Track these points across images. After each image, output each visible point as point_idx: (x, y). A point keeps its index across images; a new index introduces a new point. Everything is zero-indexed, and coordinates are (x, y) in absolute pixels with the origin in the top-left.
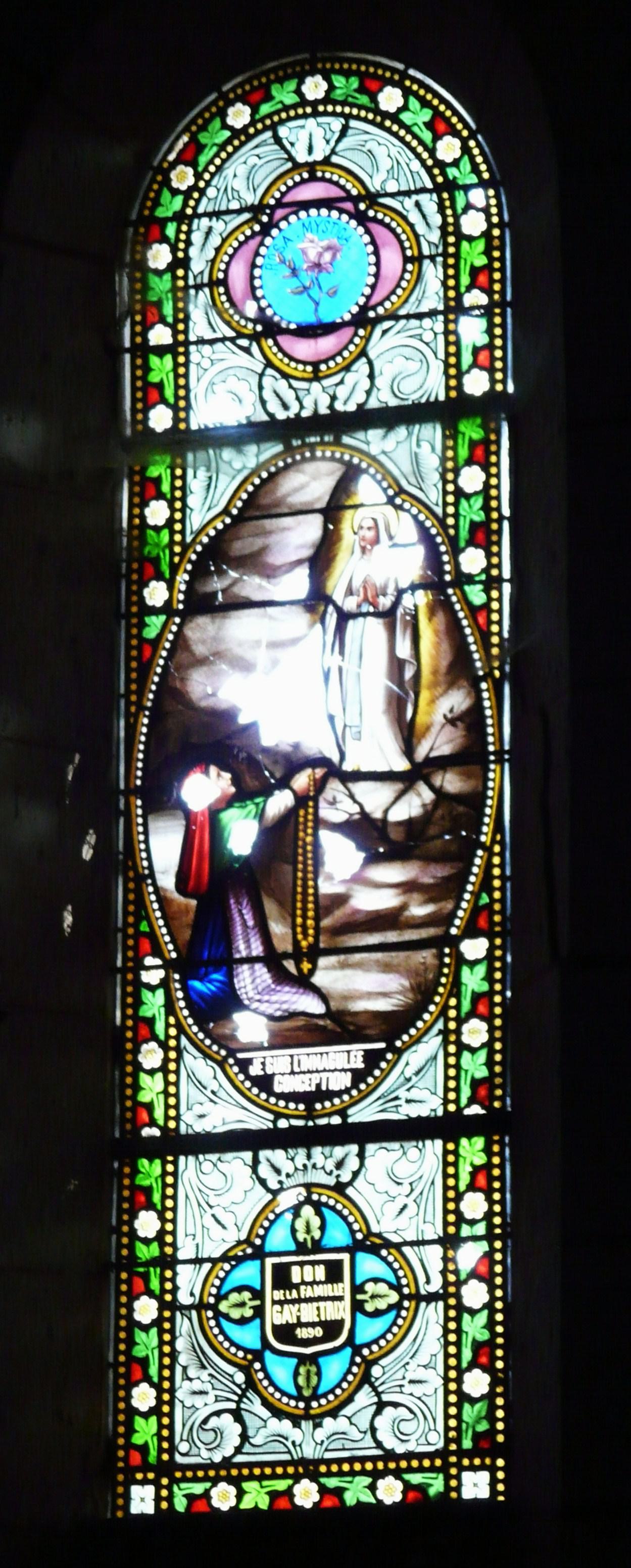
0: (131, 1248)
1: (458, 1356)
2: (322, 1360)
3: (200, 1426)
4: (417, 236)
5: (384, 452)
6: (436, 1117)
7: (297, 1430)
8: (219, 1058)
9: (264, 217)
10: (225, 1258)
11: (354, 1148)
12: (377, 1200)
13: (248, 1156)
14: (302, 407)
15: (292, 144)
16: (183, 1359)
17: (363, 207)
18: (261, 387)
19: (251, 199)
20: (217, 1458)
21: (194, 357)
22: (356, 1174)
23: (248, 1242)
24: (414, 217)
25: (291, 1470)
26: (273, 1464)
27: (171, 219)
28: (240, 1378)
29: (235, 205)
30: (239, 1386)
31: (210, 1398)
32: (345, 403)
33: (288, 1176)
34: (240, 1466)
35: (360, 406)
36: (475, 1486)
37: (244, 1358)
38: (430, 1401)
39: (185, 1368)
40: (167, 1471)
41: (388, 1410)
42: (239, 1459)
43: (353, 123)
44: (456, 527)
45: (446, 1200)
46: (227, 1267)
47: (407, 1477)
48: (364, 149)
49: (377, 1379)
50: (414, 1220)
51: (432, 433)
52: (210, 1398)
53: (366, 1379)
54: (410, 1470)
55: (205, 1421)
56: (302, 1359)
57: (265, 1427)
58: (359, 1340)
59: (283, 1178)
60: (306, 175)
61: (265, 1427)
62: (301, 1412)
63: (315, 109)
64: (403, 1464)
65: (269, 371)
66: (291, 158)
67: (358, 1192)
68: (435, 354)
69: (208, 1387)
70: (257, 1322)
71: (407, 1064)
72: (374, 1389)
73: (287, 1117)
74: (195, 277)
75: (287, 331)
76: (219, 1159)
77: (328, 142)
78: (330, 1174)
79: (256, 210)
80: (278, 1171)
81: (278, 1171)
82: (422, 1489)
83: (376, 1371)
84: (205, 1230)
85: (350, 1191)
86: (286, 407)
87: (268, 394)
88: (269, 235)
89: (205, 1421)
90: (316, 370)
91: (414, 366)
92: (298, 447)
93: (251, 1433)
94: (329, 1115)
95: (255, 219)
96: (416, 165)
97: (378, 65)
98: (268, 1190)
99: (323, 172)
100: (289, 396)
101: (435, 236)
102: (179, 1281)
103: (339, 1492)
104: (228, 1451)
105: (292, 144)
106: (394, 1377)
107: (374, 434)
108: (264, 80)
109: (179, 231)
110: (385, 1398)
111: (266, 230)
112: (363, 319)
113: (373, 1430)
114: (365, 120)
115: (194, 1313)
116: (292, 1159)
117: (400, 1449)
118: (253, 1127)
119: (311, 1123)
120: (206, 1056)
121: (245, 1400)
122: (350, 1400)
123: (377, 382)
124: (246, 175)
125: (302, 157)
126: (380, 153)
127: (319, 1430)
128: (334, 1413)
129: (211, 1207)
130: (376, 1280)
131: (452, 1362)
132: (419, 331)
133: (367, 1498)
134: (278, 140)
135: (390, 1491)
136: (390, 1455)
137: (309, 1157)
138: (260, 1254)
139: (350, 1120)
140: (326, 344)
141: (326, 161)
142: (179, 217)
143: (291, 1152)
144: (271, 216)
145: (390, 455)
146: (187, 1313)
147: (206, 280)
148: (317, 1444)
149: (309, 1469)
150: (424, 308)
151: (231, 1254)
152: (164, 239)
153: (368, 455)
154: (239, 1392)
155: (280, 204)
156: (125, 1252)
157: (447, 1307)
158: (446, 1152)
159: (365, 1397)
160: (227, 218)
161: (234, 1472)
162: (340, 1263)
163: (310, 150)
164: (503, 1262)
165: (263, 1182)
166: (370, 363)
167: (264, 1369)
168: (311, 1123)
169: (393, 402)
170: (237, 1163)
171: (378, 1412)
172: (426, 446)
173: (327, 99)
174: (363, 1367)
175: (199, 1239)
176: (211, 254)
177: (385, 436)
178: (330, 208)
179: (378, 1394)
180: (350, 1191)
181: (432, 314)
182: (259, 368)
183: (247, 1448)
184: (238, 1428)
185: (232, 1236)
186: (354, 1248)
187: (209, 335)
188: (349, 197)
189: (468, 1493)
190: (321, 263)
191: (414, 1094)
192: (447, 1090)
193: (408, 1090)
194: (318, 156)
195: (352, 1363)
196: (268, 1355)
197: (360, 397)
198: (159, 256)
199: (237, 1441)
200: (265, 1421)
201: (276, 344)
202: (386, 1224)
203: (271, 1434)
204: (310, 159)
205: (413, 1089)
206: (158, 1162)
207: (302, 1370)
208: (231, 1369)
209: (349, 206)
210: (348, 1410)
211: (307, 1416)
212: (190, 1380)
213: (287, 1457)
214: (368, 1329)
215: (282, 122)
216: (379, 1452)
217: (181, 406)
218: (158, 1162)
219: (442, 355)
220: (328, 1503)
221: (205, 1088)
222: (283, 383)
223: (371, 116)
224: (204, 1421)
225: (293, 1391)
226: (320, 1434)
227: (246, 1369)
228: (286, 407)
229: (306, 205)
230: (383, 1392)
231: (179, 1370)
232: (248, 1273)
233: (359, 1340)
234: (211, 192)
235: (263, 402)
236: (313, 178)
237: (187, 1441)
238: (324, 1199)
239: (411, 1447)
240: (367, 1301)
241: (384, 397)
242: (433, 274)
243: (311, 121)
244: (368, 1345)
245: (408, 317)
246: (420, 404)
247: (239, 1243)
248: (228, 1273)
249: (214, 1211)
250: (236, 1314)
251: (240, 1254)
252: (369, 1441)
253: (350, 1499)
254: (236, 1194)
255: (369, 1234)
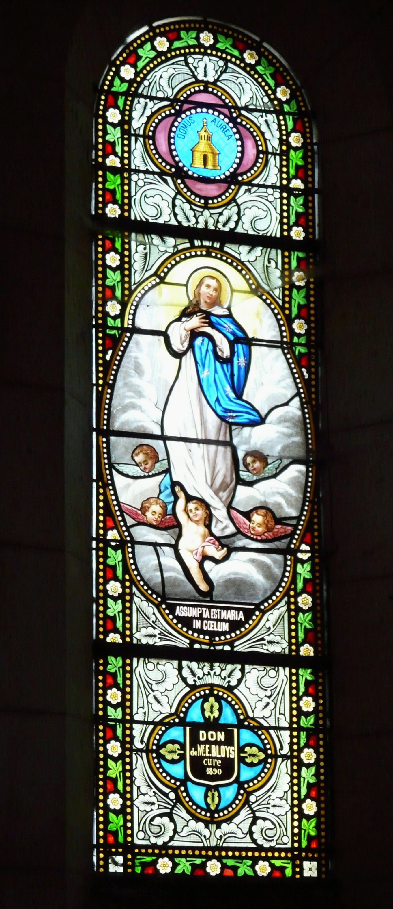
0: (105, 710)
1: (299, 792)
2: (221, 789)
3: (150, 823)
4: (265, 140)
5: (249, 261)
6: (284, 655)
7: (207, 830)
8: (156, 602)
9: (179, 105)
10: (161, 723)
11: (239, 666)
12: (253, 700)
13: (176, 663)
14: (197, 222)
15: (196, 68)
16: (138, 782)
17: (234, 115)
18: (174, 206)
19: (170, 93)
20: (160, 842)
21: (134, 177)
22: (240, 681)
23: (176, 714)
24: (264, 128)
25: (204, 853)
26: (193, 849)
27: (122, 94)
28: (172, 796)
29: (160, 95)
30: (172, 801)
31: (155, 807)
32: (224, 225)
33: (199, 678)
34: (174, 848)
35: (232, 230)
36: (310, 869)
37: (175, 784)
38: (283, 818)
39: (139, 788)
40: (296, 856)
41: (259, 822)
42: (173, 843)
43: (230, 65)
44: (290, 309)
45: (291, 702)
46: (163, 728)
47: (225, 861)
48: (237, 82)
49: (253, 803)
50: (273, 712)
51: (276, 254)
52: (155, 807)
53: (247, 802)
54: (227, 857)
55: (152, 819)
56: (209, 788)
57: (187, 826)
58: (243, 778)
59: (196, 679)
60: (202, 88)
61: (187, 826)
62: (209, 819)
63: (203, 51)
64: (270, 854)
65: (179, 197)
66: (194, 76)
67: (241, 692)
68: (275, 209)
69: (154, 800)
70: (182, 762)
71: (268, 620)
72: (251, 809)
73: (200, 643)
74: (135, 131)
75: (191, 177)
76: (158, 663)
77: (216, 71)
78: (225, 679)
79: (174, 101)
80: (194, 674)
81: (194, 674)
82: (282, 869)
83: (252, 798)
84: (150, 705)
85: (236, 691)
86: (189, 221)
87: (177, 210)
88: (230, 121)
89: (152, 819)
90: (206, 203)
91: (263, 214)
92: (198, 247)
93: (179, 829)
94: (224, 644)
95: (172, 106)
96: (266, 99)
97: (244, 35)
98: (187, 685)
99: (213, 89)
100: (191, 214)
101: (276, 143)
102: (135, 733)
103: (235, 869)
104: (166, 838)
105: (196, 68)
106: (263, 803)
107: (244, 249)
108: (177, 27)
109: (125, 104)
110: (258, 814)
111: (178, 114)
112: (232, 180)
113: (251, 833)
114: (234, 63)
115: (144, 755)
116: (202, 669)
117: (266, 845)
118: (180, 645)
119: (212, 648)
120: (148, 600)
121: (175, 809)
122: (237, 814)
123: (243, 218)
124: (167, 79)
125: (201, 77)
126: (247, 87)
127: (218, 830)
128: (229, 820)
129: (153, 691)
130: (251, 745)
131: (296, 795)
132: (266, 195)
133: (250, 873)
134: (187, 64)
135: (263, 869)
136: (260, 848)
137: (212, 668)
138: (183, 723)
139: (235, 649)
140: (211, 190)
141: (215, 83)
142: (126, 94)
143: (202, 665)
144: (181, 107)
145: (252, 263)
146: (139, 753)
147: (141, 133)
148: (218, 839)
149: (216, 852)
150: (268, 183)
151: (166, 721)
152: (116, 107)
153: (239, 260)
154: (172, 804)
155: (186, 101)
156: (101, 713)
157: (292, 764)
158: (291, 674)
159: (245, 812)
160: (156, 101)
161: (170, 852)
162: (233, 731)
163: (205, 76)
164: (98, 738)
165: (184, 680)
166: (238, 206)
167: (186, 790)
168: (212, 648)
169: (251, 232)
170: (170, 667)
171: (253, 823)
172: (273, 264)
173: (213, 47)
174: (245, 795)
175: (146, 709)
176: (144, 119)
177: (250, 251)
178: (214, 110)
179: (253, 812)
180: (236, 691)
181: (273, 187)
182: (173, 194)
183: (177, 837)
184: (171, 826)
185: (166, 710)
186: (240, 725)
187: (143, 168)
188: (226, 106)
189: (306, 874)
190: (205, 142)
191: (271, 638)
192: (290, 637)
193: (268, 635)
194: (210, 79)
195: (238, 793)
196: (189, 784)
197: (232, 225)
198: (114, 115)
199: (171, 833)
200: (188, 822)
201: (183, 182)
202: (258, 713)
203: (191, 832)
204: (205, 79)
205: (271, 635)
206: (120, 659)
207: (210, 794)
208: (167, 790)
209: (226, 111)
210: (237, 820)
211: (212, 822)
212: (144, 795)
213: (201, 845)
214: (246, 774)
215: (190, 54)
216: (253, 845)
217: (126, 205)
218: (120, 659)
219: (279, 210)
220: (277, 874)
221: (146, 254)
222: (187, 207)
223: (238, 62)
224: (152, 816)
225: (204, 806)
226: (218, 833)
227: (175, 790)
228: (189, 221)
229: (202, 105)
230: (256, 811)
231: (135, 789)
232: (176, 733)
233: (243, 778)
234: (146, 83)
235: (175, 215)
236: (205, 91)
237: (142, 831)
238: (221, 694)
239: (273, 844)
240: (247, 757)
241: (245, 227)
242: (274, 162)
243: (206, 58)
244: (247, 782)
245: (259, 186)
246: (266, 236)
247: (171, 715)
248: (164, 732)
249: (155, 693)
250: (169, 757)
251: (172, 721)
252: (248, 839)
253: (240, 873)
254: (168, 685)
255: (247, 717)
